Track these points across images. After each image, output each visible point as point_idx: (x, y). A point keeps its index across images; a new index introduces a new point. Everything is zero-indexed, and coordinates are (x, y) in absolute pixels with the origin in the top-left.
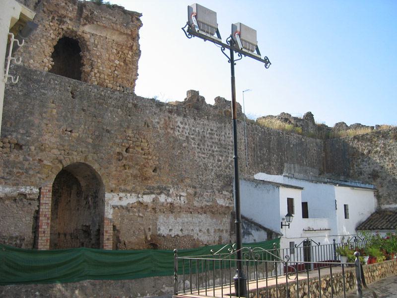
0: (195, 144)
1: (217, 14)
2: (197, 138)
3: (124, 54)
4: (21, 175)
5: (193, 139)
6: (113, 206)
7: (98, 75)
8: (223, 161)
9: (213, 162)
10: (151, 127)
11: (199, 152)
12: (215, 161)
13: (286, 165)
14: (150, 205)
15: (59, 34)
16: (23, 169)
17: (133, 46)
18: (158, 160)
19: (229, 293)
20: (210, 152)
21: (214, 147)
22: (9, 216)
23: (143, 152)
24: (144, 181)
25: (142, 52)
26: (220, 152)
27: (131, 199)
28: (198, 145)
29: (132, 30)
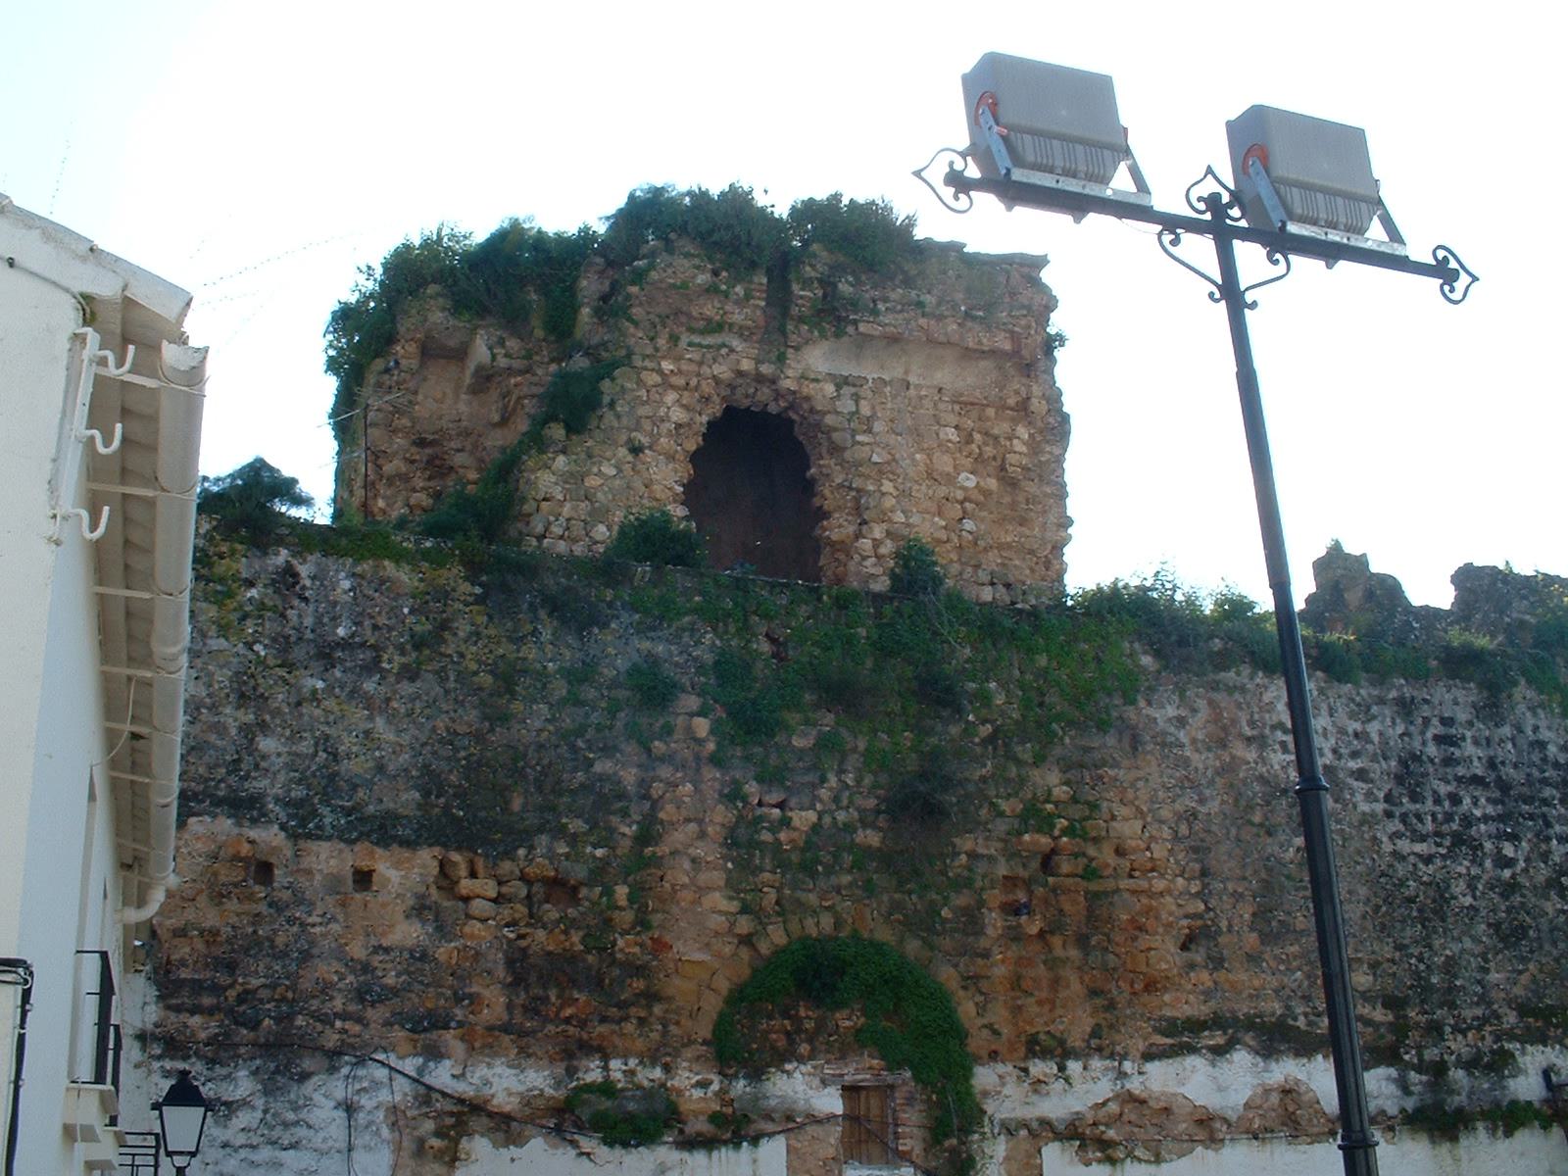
0: (1369, 796)
1: (1234, 114)
2: (1377, 769)
3: (996, 438)
5: (1361, 775)
8: (1522, 864)
15: (706, 399)
19: (152, 1169)
23: (1126, 864)
24: (1145, 998)
29: (1012, 332)
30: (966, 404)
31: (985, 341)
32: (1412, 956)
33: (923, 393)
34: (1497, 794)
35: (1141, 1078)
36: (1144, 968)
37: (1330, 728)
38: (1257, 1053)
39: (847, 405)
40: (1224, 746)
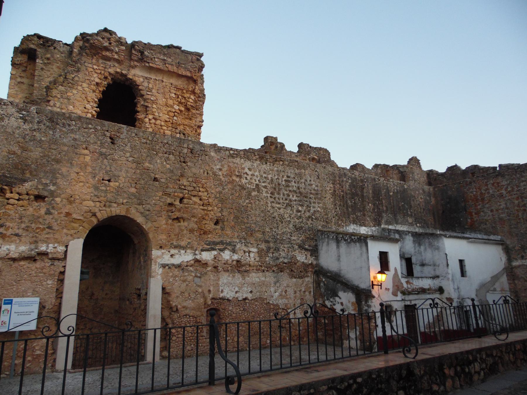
0: (267, 192)
3: (185, 98)
4: (42, 231)
5: (265, 187)
6: (162, 264)
7: (153, 121)
8: (303, 212)
9: (291, 212)
10: (211, 175)
11: (273, 202)
12: (293, 211)
13: (384, 215)
14: (211, 263)
16: (44, 225)
17: (195, 89)
18: (220, 212)
20: (287, 202)
21: (291, 196)
22: (24, 280)
23: (201, 203)
24: (203, 236)
25: (206, 96)
26: (300, 201)
27: (186, 257)
28: (272, 193)
30: (178, 89)
31: (184, 72)
32: (273, 231)
33: (167, 84)
34: (299, 195)
35: (200, 255)
36: (203, 228)
37: (258, 175)
38: (231, 251)
39: (146, 84)
40: (231, 177)
